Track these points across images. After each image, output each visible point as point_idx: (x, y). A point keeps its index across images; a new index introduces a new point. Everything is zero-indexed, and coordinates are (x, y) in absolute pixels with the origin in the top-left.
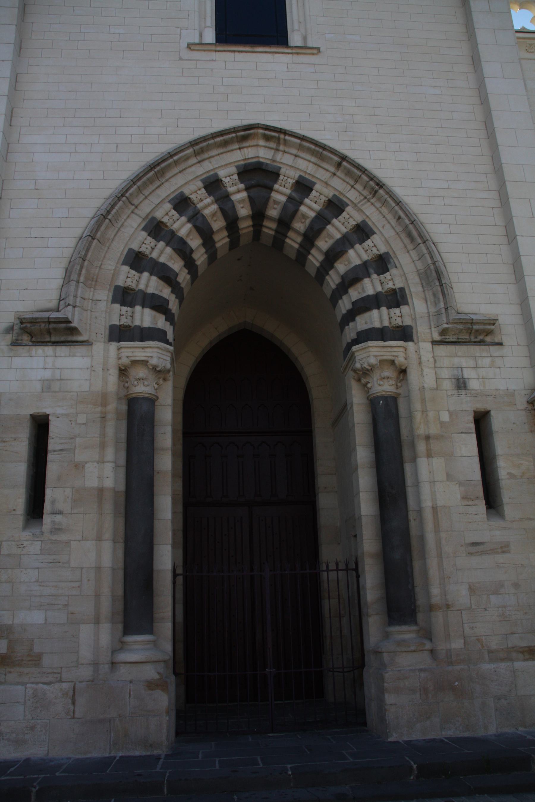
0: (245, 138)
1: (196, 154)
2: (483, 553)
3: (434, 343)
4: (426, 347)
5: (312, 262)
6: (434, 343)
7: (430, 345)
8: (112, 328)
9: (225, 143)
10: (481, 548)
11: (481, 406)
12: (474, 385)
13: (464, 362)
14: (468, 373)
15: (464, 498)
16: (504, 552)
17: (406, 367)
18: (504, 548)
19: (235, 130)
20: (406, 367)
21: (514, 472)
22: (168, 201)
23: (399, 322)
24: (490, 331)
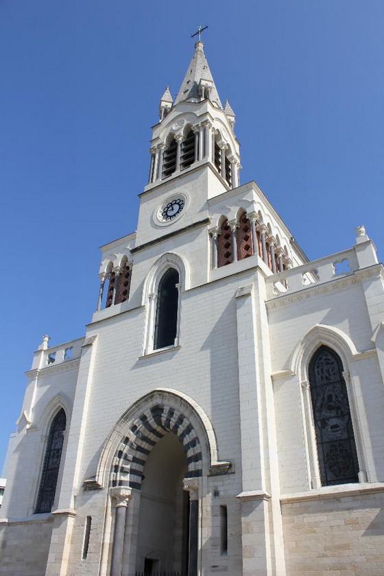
0: (152, 396)
1: (137, 407)
2: (218, 571)
3: (208, 476)
4: (205, 478)
5: (40, 359)
6: (208, 476)
7: (206, 477)
8: (192, 428)
9: (146, 400)
10: (216, 568)
11: (223, 503)
12: (221, 493)
13: (216, 484)
14: (220, 489)
15: (213, 546)
16: (225, 571)
17: (134, 367)
18: (225, 569)
19: (148, 395)
20: (134, 367)
21: (233, 533)
22: (203, 453)
23: (150, 413)
24: (297, 505)
